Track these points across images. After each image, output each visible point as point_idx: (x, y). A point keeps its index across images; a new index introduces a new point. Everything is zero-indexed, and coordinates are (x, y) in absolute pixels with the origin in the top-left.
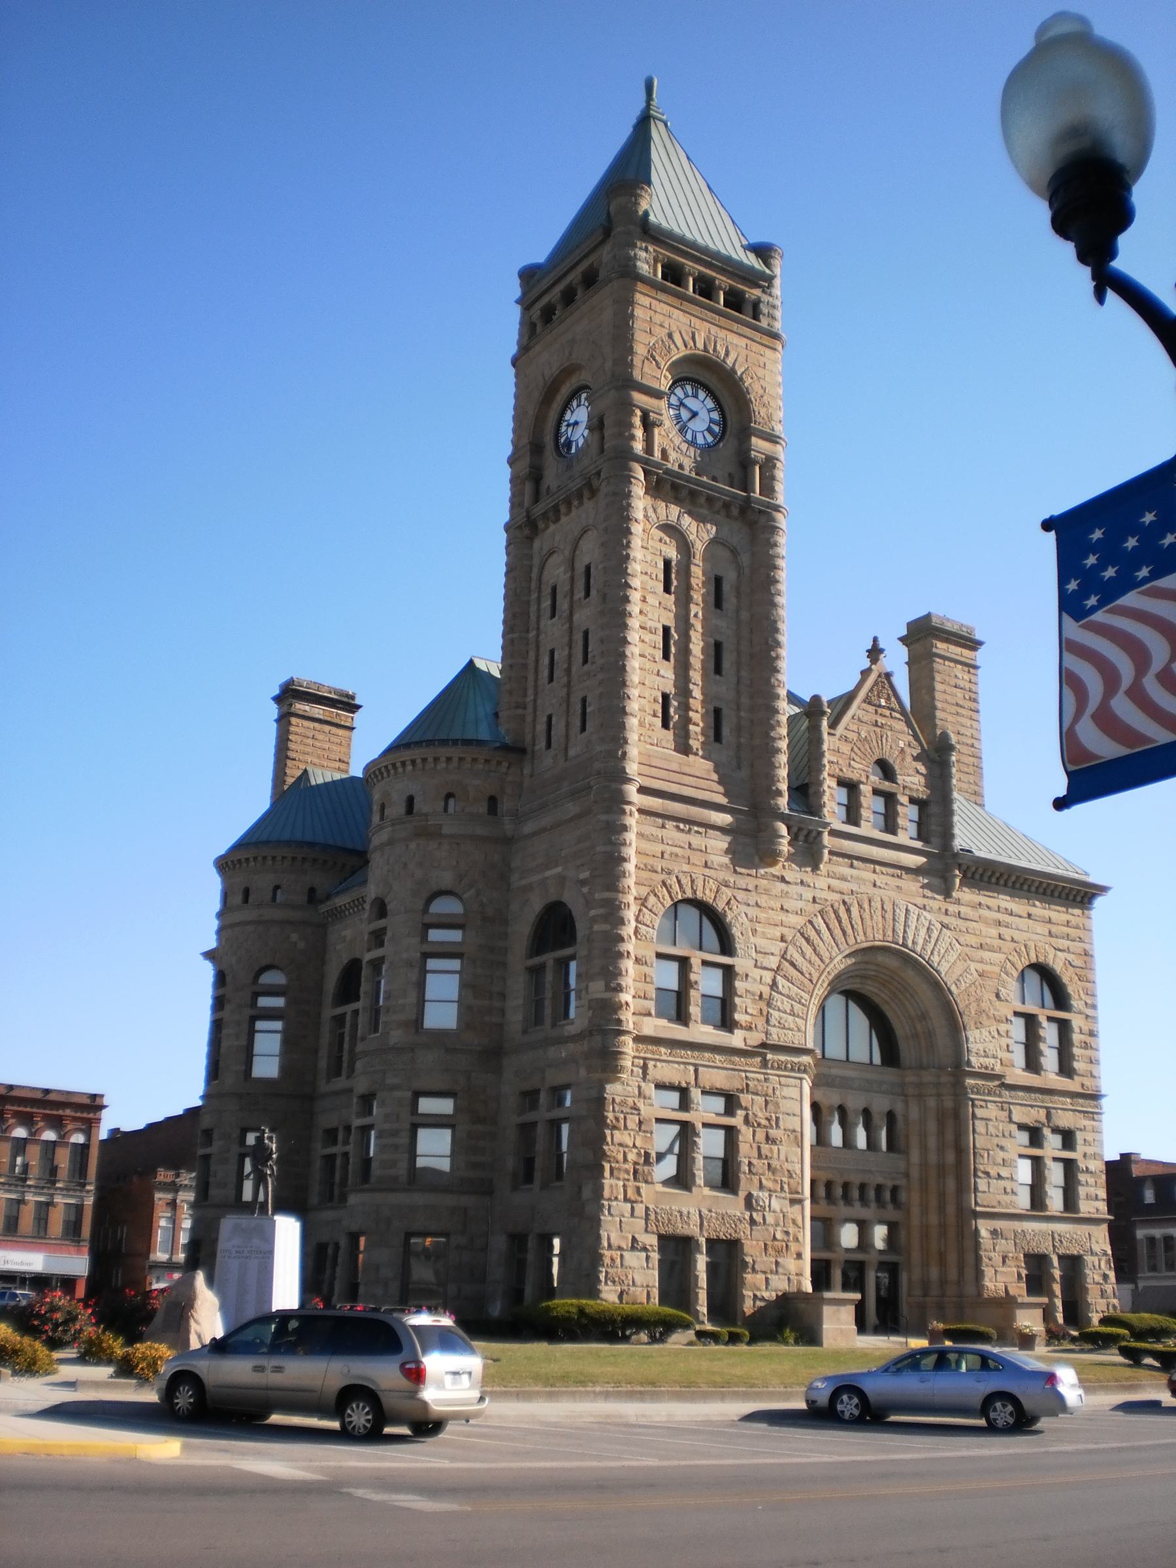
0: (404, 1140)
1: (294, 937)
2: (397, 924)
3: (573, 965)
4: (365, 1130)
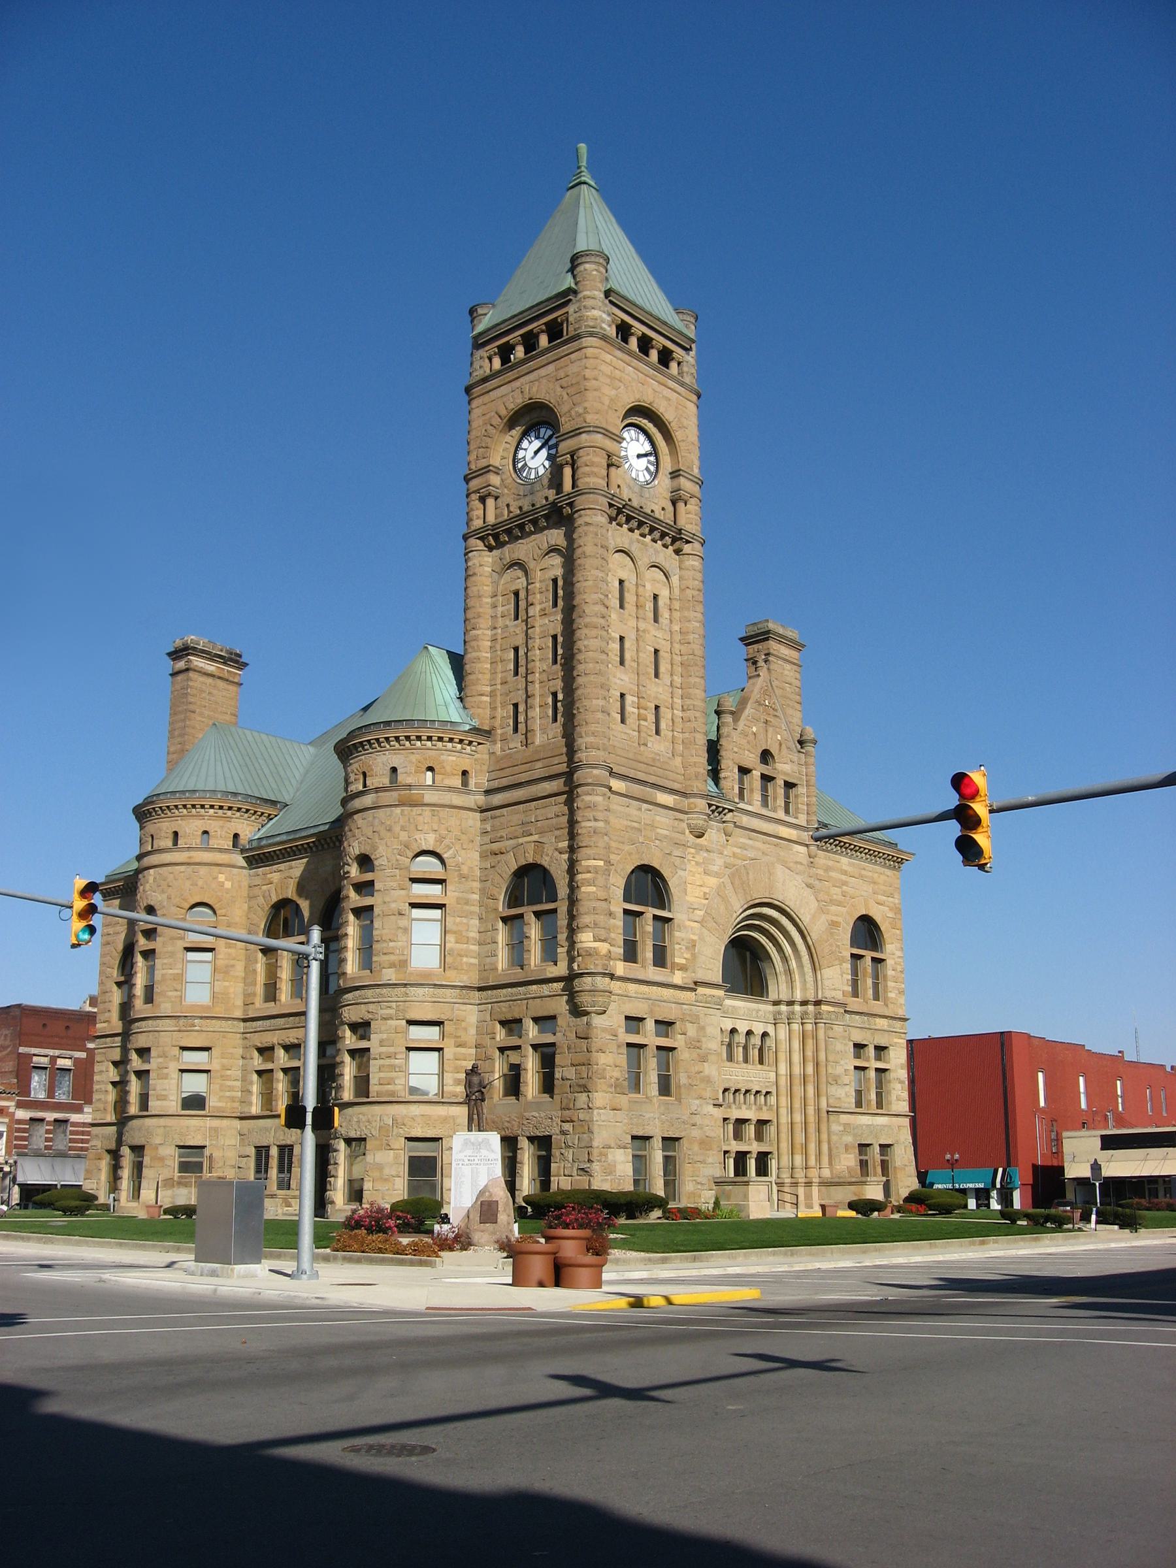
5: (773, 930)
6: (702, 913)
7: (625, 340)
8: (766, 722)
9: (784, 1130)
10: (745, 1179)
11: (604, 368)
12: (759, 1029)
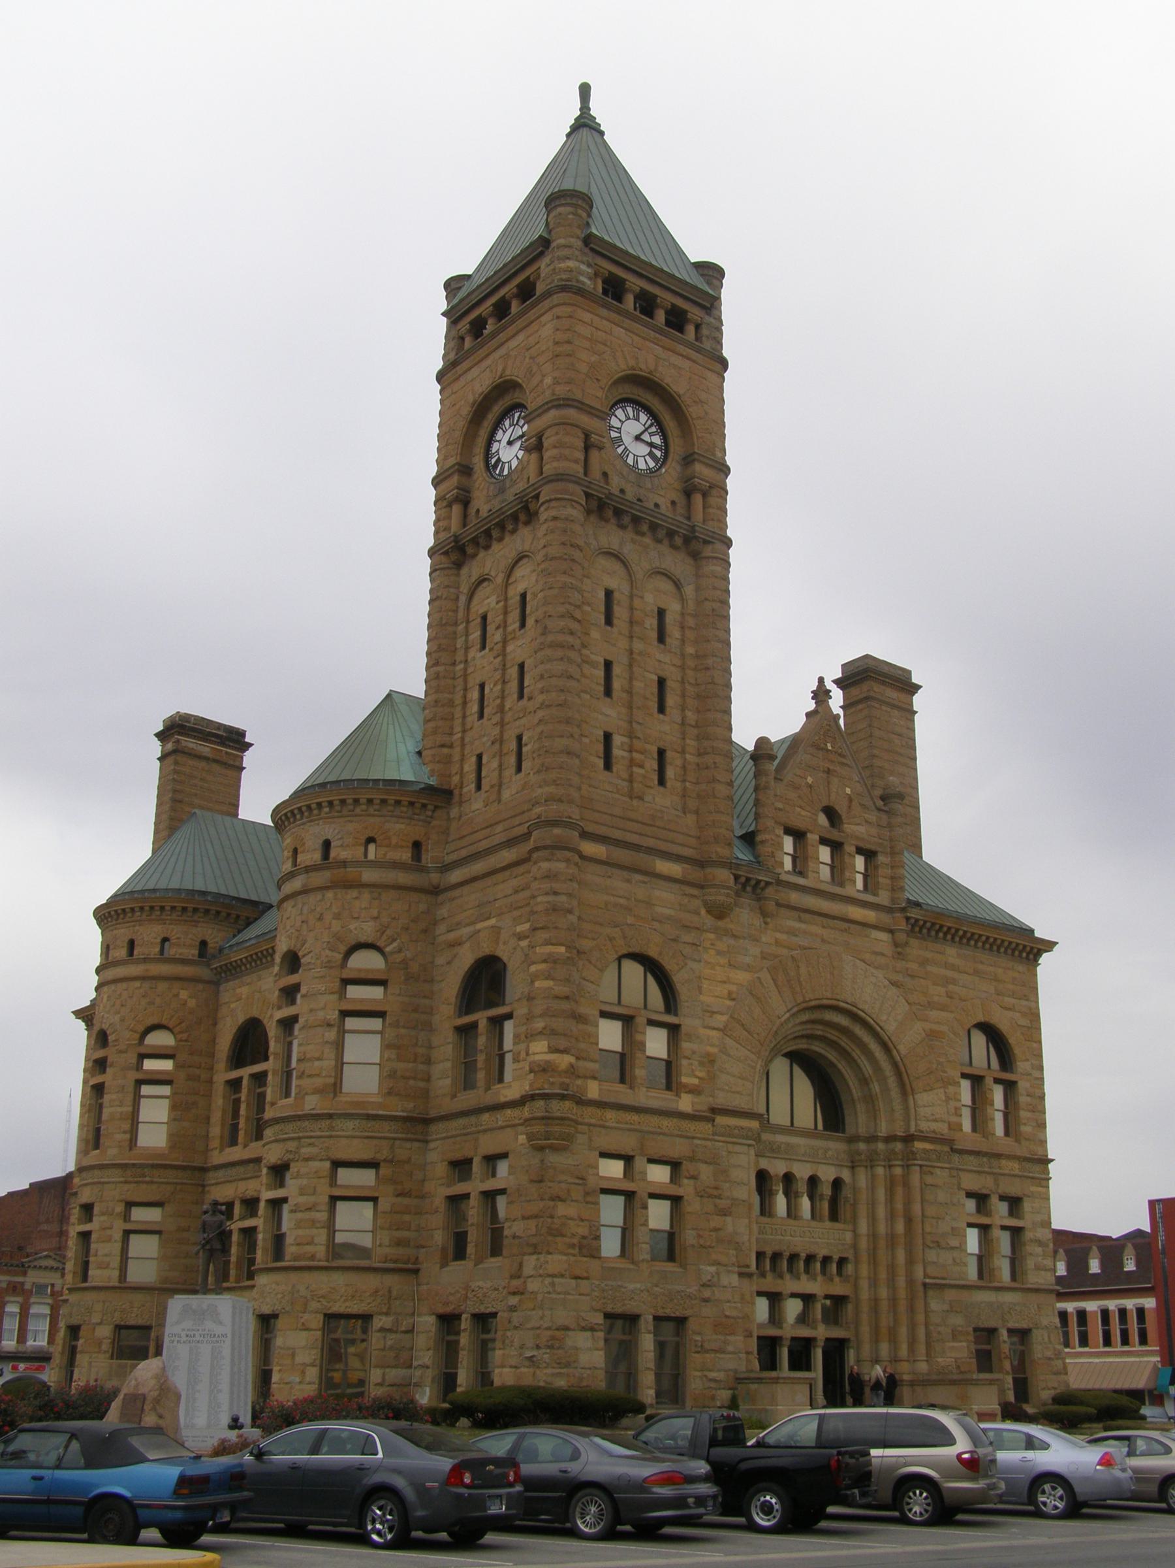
0: (323, 1216)
1: (184, 994)
2: (310, 979)
3: (509, 1026)
4: (277, 1204)
5: (844, 1042)
6: (725, 1018)
7: (619, 298)
8: (828, 771)
9: (865, 1308)
10: (774, 1374)
11: (580, 328)
12: (827, 1174)
